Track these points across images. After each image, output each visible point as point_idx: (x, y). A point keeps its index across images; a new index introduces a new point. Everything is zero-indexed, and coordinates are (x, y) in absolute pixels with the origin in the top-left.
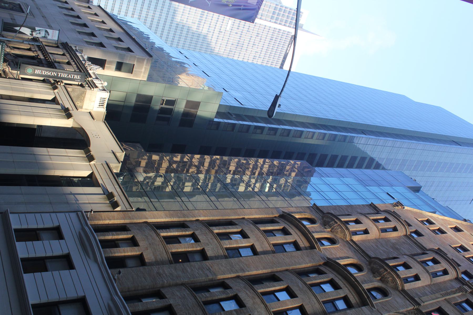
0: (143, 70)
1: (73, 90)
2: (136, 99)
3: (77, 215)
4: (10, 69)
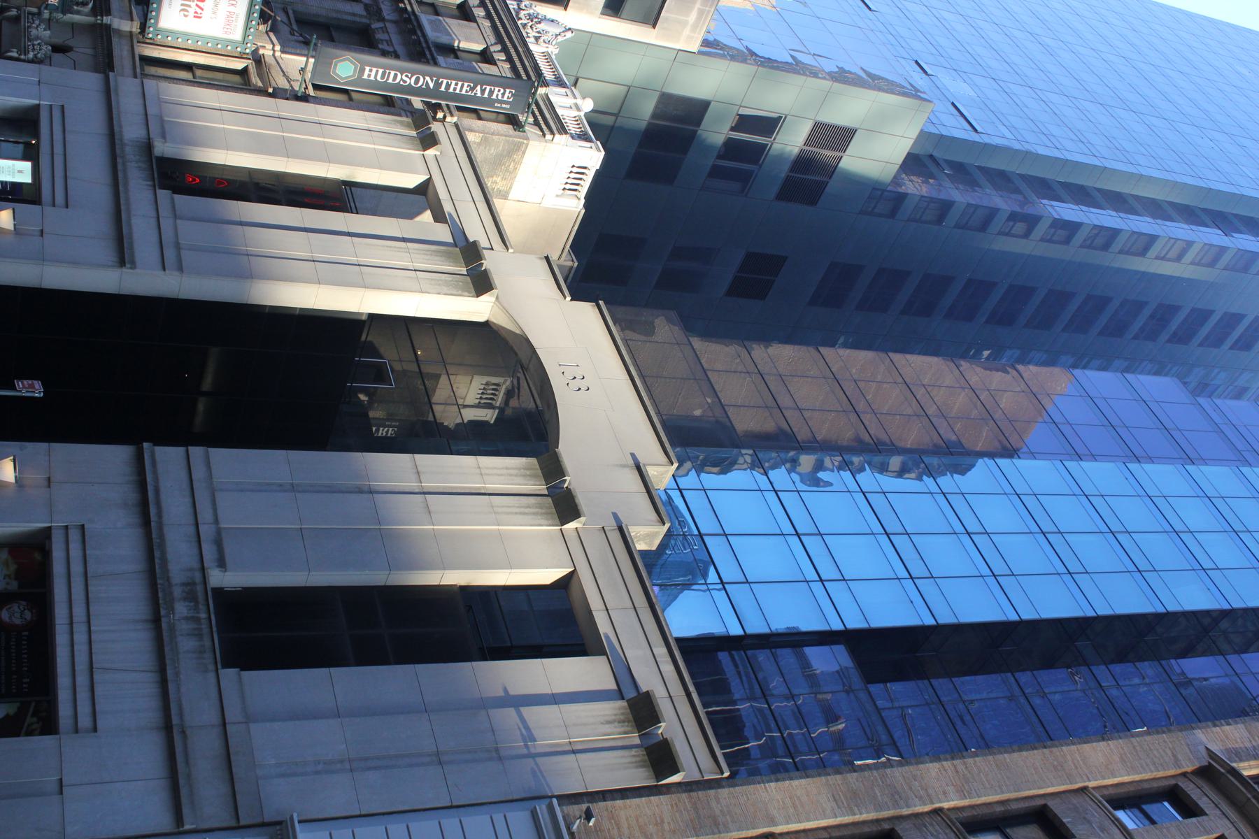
0: (693, 17)
1: (485, 141)
2: (656, 107)
3: (534, 814)
4: (278, 48)
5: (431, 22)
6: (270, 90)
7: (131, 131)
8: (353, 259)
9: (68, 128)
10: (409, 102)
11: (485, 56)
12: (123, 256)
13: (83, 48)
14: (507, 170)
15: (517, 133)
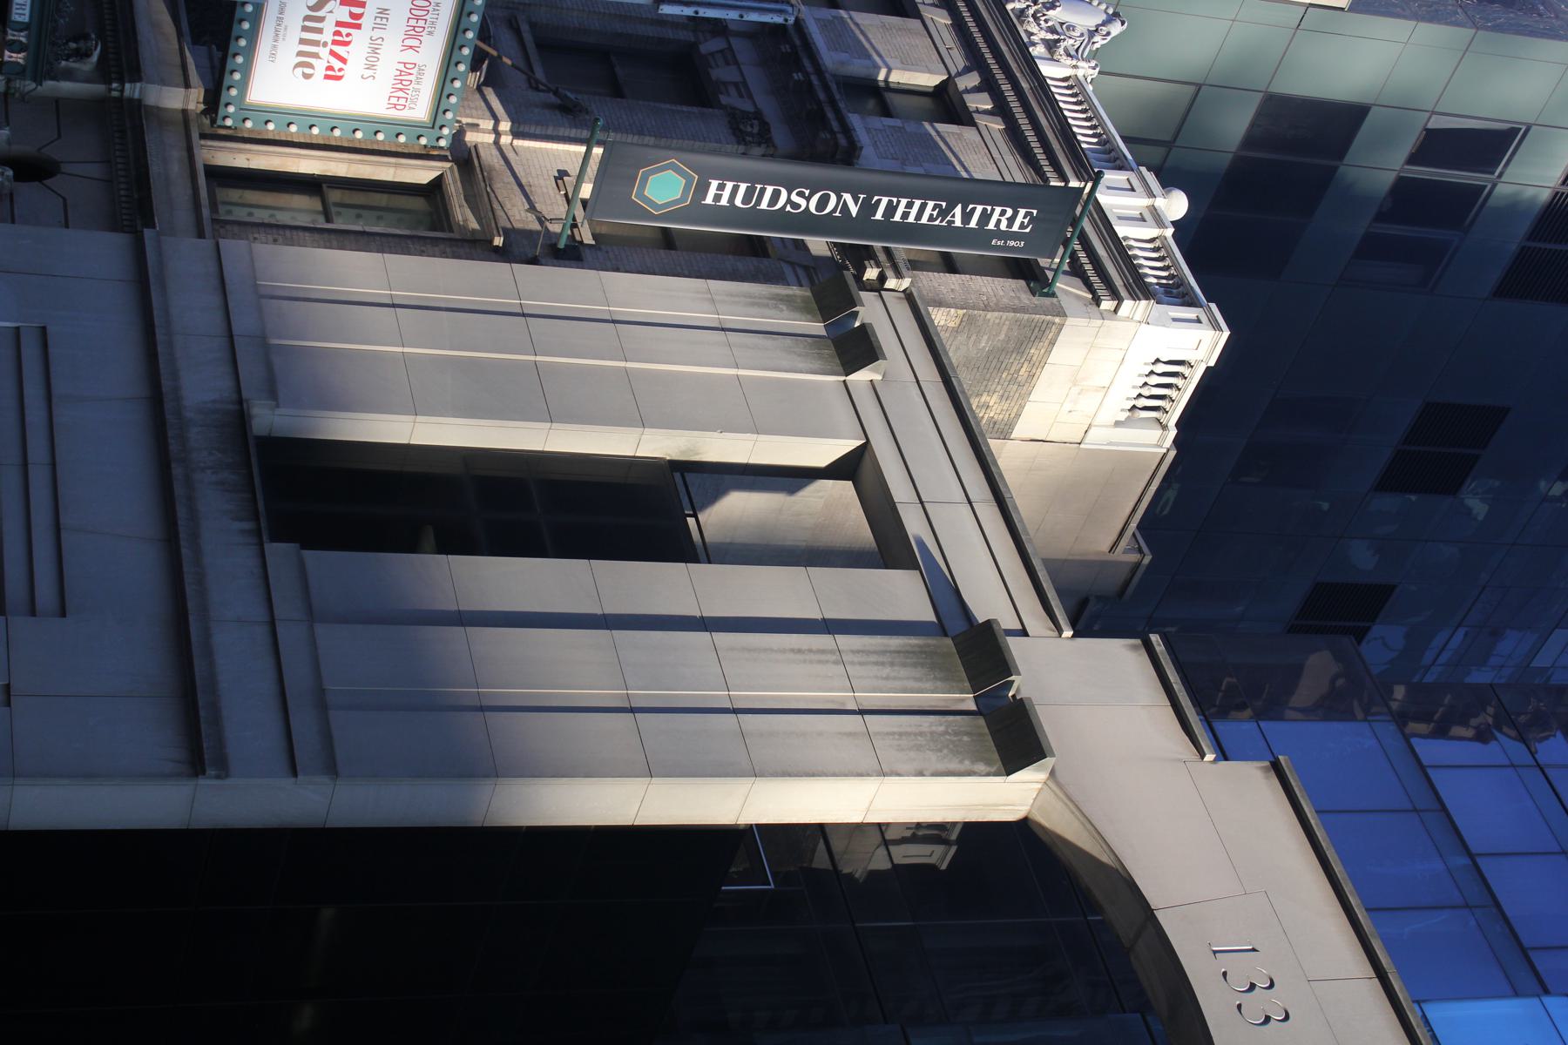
1: (968, 323)
2: (1253, 125)
4: (505, 126)
5: (825, 25)
6: (498, 241)
7: (200, 385)
8: (719, 696)
9: (59, 387)
10: (801, 245)
11: (945, 104)
12: (200, 752)
13: (82, 166)
14: (1013, 380)
15: (1037, 300)
